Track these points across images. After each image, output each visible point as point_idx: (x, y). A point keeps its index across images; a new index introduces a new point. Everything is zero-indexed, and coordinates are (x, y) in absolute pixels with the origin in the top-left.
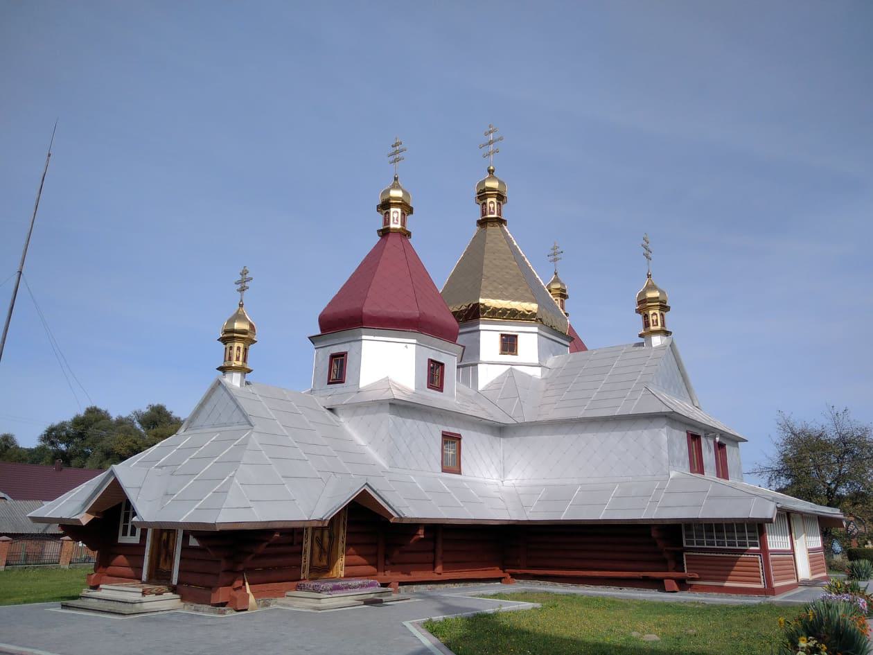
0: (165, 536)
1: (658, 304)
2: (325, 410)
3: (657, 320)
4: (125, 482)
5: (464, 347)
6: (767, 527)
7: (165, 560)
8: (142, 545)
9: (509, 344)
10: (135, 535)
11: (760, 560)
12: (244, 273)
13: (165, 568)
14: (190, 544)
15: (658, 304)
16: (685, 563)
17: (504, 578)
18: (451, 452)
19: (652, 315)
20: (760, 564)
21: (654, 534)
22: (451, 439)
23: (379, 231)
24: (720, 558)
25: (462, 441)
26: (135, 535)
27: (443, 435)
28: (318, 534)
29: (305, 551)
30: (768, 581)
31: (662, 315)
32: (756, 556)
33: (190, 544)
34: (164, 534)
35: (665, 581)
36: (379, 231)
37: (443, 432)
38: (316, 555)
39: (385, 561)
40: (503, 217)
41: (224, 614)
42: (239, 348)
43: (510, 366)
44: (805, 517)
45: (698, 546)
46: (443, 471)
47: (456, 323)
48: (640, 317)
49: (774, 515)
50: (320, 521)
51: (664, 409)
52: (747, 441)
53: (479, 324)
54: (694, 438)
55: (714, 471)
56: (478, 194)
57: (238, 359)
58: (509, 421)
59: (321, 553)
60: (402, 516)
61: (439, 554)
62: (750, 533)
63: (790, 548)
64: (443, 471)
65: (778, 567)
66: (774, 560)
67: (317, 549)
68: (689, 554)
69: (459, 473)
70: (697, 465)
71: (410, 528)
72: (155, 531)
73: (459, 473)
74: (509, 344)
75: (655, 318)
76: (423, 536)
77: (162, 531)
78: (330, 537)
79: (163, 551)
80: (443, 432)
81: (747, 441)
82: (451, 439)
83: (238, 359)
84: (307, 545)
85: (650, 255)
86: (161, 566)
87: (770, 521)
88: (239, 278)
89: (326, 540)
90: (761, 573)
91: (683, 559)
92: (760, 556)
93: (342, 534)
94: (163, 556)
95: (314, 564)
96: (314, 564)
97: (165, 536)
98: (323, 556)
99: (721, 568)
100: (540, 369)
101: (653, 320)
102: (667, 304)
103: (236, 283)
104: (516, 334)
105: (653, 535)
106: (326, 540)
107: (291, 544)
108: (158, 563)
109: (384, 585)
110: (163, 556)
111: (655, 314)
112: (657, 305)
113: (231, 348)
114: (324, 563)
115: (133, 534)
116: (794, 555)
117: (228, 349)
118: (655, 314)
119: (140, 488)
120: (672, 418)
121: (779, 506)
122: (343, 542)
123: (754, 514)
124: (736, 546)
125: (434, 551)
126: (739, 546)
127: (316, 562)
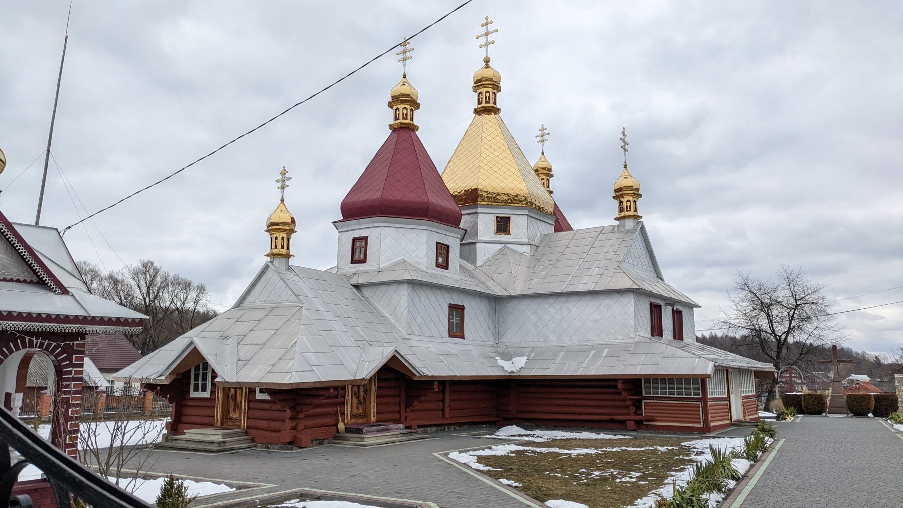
0: (232, 391)
1: (632, 192)
2: (352, 287)
3: (630, 206)
4: (205, 349)
5: (466, 230)
6: (708, 382)
7: (234, 410)
8: (211, 400)
9: (503, 225)
10: (205, 391)
11: (701, 406)
12: (284, 172)
13: (234, 416)
14: (257, 398)
15: (632, 192)
16: (643, 408)
17: (497, 421)
18: (455, 320)
19: (627, 201)
20: (701, 408)
21: (620, 386)
22: (457, 311)
23: (390, 126)
24: (683, 405)
25: (465, 311)
26: (205, 391)
27: (449, 307)
28: (355, 389)
29: (347, 402)
30: (706, 421)
31: (635, 201)
32: (698, 403)
33: (257, 398)
34: (231, 391)
35: (627, 422)
36: (390, 126)
37: (450, 304)
38: (355, 405)
39: (406, 409)
40: (498, 106)
41: (293, 450)
42: (283, 238)
43: (504, 245)
44: (741, 371)
45: (661, 396)
46: (450, 336)
47: (455, 206)
48: (616, 202)
49: (712, 372)
50: (363, 379)
51: (634, 286)
52: (701, 307)
53: (477, 208)
54: (656, 311)
55: (671, 333)
56: (475, 83)
57: (283, 247)
58: (505, 294)
59: (358, 404)
60: (423, 375)
61: (448, 401)
62: (681, 387)
63: (726, 396)
64: (450, 336)
65: (750, 410)
66: (712, 405)
67: (355, 400)
68: (647, 401)
69: (463, 338)
70: (657, 330)
71: (428, 384)
72: (224, 388)
73: (463, 338)
74: (503, 225)
75: (628, 204)
76: (437, 390)
77: (229, 389)
78: (364, 391)
79: (232, 403)
80: (450, 304)
81: (701, 307)
82: (457, 311)
83: (283, 247)
84: (348, 398)
85: (627, 147)
86: (231, 415)
87: (709, 376)
88: (280, 177)
89: (362, 393)
90: (701, 416)
91: (642, 405)
92: (701, 402)
93: (374, 388)
94: (232, 407)
95: (353, 412)
96: (353, 412)
97: (232, 391)
98: (360, 406)
99: (572, 402)
100: (529, 246)
101: (627, 206)
102: (640, 192)
103: (276, 181)
104: (509, 216)
105: (618, 387)
106: (362, 393)
107: (337, 397)
108: (228, 413)
109: (407, 428)
110: (232, 407)
111: (628, 201)
112: (631, 193)
113: (276, 238)
114: (361, 411)
115: (204, 389)
116: (730, 401)
117: (274, 239)
118: (628, 201)
119: (216, 354)
120: (638, 293)
121: (717, 364)
122: (374, 395)
123: (698, 371)
124: (675, 395)
125: (443, 401)
126: (669, 394)
127: (355, 411)
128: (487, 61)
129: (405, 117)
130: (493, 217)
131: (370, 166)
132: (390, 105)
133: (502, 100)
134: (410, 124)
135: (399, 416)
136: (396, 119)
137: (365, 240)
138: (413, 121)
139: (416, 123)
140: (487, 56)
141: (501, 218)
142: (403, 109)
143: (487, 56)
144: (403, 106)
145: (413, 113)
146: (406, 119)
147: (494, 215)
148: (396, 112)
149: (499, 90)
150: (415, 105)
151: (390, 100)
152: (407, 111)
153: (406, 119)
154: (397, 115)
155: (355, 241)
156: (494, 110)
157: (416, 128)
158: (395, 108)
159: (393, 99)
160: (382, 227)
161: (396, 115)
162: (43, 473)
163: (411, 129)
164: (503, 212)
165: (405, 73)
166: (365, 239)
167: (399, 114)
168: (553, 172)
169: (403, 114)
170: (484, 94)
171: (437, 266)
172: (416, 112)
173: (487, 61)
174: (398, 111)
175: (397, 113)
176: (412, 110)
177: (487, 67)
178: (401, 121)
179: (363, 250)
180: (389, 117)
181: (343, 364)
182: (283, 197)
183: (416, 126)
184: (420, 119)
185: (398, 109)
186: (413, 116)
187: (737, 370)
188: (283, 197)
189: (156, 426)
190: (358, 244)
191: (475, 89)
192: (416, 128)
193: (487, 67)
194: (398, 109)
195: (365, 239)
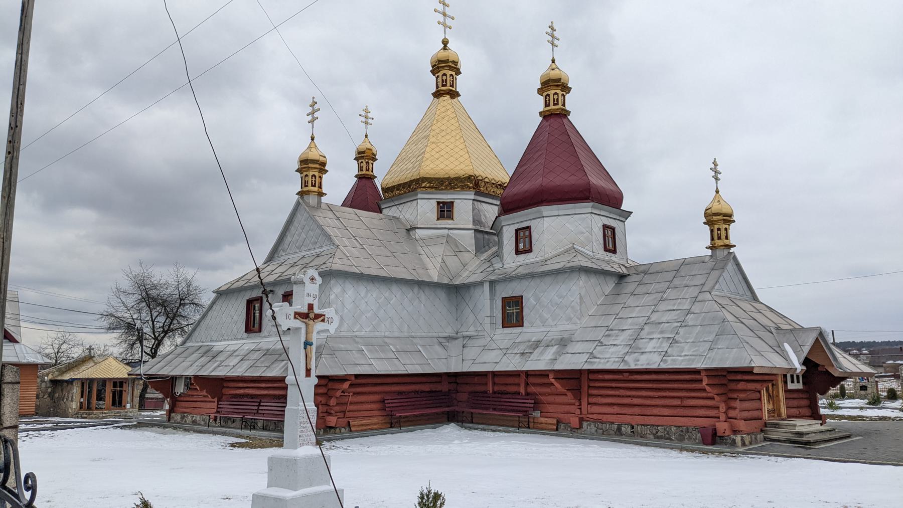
9: (445, 210)
33: (789, 388)
74: (445, 210)
104: (452, 200)
128: (445, 43)
129: (556, 102)
130: (434, 203)
131: (525, 154)
132: (540, 91)
133: (462, 83)
134: (562, 109)
135: (589, 400)
136: (547, 105)
137: (528, 229)
138: (564, 106)
139: (568, 107)
140: (445, 38)
141: (444, 203)
142: (554, 94)
143: (445, 38)
144: (553, 92)
145: (564, 98)
146: (557, 104)
147: (436, 200)
148: (546, 98)
149: (458, 72)
150: (566, 89)
151: (539, 86)
152: (558, 96)
153: (557, 104)
154: (548, 101)
155: (519, 231)
156: (454, 94)
157: (569, 113)
158: (545, 94)
159: (542, 86)
160: (545, 218)
161: (546, 101)
162: (28, 500)
163: (564, 114)
164: (446, 197)
165: (553, 58)
166: (529, 228)
167: (549, 100)
168: (377, 157)
169: (554, 99)
170: (440, 77)
171: (605, 250)
172: (567, 96)
173: (445, 43)
174: (548, 97)
175: (548, 99)
176: (563, 95)
177: (445, 48)
178: (552, 107)
179: (527, 240)
180: (539, 104)
181: (800, 346)
182: (717, 189)
183: (567, 111)
184: (571, 102)
185: (548, 95)
186: (564, 100)
187: (789, 331)
188: (717, 189)
189: (24, 441)
190: (522, 234)
191: (434, 72)
192: (569, 113)
193: (445, 48)
194: (548, 95)
195: (529, 228)
